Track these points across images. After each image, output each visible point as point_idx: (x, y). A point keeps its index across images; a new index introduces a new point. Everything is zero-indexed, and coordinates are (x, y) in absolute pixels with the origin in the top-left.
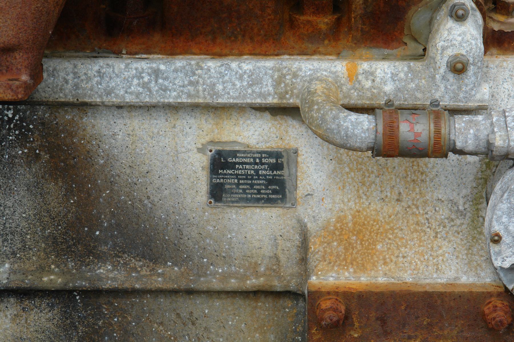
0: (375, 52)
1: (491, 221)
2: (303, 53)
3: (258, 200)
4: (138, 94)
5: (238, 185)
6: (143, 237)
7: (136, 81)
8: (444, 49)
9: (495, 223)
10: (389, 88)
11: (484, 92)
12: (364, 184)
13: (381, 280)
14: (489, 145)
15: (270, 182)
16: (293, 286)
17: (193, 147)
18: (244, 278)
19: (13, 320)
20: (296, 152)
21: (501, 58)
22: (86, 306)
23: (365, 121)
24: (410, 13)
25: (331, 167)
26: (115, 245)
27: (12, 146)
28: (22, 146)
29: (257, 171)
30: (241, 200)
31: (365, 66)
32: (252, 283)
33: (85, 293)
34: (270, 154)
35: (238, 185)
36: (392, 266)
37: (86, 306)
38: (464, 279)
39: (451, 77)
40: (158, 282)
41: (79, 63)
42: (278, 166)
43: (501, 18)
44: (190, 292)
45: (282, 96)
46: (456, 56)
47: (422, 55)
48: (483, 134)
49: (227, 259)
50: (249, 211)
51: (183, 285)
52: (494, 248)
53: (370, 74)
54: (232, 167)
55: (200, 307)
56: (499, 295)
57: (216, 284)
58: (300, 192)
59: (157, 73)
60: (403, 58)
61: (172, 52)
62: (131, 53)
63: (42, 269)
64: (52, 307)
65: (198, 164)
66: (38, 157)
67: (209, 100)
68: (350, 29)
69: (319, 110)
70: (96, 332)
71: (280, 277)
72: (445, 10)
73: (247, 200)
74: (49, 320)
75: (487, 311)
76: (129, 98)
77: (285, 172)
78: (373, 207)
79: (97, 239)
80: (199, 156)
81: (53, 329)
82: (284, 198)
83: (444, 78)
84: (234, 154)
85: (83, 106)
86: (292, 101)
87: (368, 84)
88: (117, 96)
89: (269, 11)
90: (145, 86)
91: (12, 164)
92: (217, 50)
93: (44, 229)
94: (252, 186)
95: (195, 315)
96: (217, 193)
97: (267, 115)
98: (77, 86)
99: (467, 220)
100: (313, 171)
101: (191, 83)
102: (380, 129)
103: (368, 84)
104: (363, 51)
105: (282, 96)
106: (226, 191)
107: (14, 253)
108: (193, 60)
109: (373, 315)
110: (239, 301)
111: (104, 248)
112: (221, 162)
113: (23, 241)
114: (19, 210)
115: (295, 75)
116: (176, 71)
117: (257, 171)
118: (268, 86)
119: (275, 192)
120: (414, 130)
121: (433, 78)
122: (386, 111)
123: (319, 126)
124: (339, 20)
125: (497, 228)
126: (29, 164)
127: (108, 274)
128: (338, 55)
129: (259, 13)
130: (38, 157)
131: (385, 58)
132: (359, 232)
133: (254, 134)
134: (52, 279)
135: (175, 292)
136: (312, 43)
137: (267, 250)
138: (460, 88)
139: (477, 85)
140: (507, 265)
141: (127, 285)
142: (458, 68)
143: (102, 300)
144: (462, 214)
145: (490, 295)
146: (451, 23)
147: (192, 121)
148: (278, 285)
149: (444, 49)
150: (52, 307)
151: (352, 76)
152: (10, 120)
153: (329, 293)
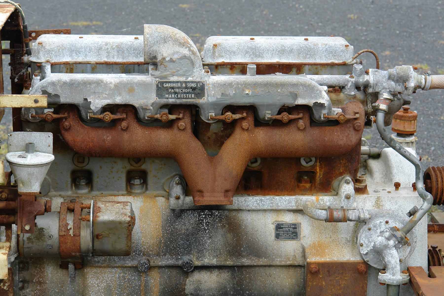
0: (323, 194)
1: (360, 240)
2: (302, 195)
3: (290, 238)
4: (256, 207)
5: (284, 234)
6: (256, 250)
7: (255, 203)
8: (344, 192)
9: (361, 240)
10: (328, 204)
11: (355, 205)
12: (320, 233)
13: (328, 260)
14: (359, 218)
15: (293, 233)
16: (301, 263)
17: (270, 223)
18: (286, 262)
19: (217, 276)
20: (300, 224)
21: (359, 195)
22: (238, 271)
23: (324, 212)
24: (333, 182)
25: (311, 228)
26: (247, 253)
27: (217, 223)
28: (220, 223)
29: (289, 230)
30: (285, 238)
31: (321, 197)
32: (288, 263)
33: (238, 267)
34: (293, 224)
35: (284, 234)
36: (331, 256)
37: (238, 271)
38: (352, 259)
39: (346, 200)
40: (261, 263)
41: (239, 198)
42: (295, 228)
43: (358, 184)
44: (270, 266)
45: (297, 207)
46: (347, 194)
47: (337, 194)
48: (357, 215)
49: (280, 256)
50: (287, 242)
51: (268, 264)
52: (361, 248)
53: (322, 200)
54: (282, 228)
55: (273, 271)
56: (362, 263)
57: (278, 263)
58: (302, 236)
59: (261, 200)
60: (331, 195)
61: (264, 195)
62: (253, 195)
63: (226, 260)
64: (228, 272)
65: (271, 228)
66: (225, 226)
67: (276, 208)
68: (315, 187)
69: (310, 209)
70: (241, 279)
71: (297, 261)
72: (343, 181)
73: (286, 238)
74: (228, 276)
75: (359, 267)
76: (253, 208)
77: (297, 230)
78: (323, 240)
79: (242, 251)
80: (272, 225)
81: (229, 279)
82: (297, 238)
83: (344, 200)
84: (282, 224)
85: (239, 210)
86: (300, 208)
87: (322, 203)
88: (250, 207)
89: (292, 182)
90: (258, 204)
91: (217, 228)
92: (277, 194)
93: (226, 248)
94: (288, 234)
95: (271, 274)
96: (277, 236)
97: (292, 213)
98: (238, 204)
99: (351, 243)
100: (306, 228)
101: (271, 203)
102: (328, 214)
103: (322, 203)
104: (319, 194)
105: (297, 207)
106: (280, 236)
107: (217, 256)
108: (272, 197)
109: (326, 270)
110: (284, 269)
111: (244, 254)
112: (279, 227)
113: (220, 252)
114: (219, 242)
115: (301, 200)
116: (267, 199)
117: (289, 230)
118: (293, 204)
119: (294, 236)
120: (337, 214)
121: (341, 200)
122: (330, 210)
123: (310, 214)
124: (312, 185)
125: (362, 242)
126: (222, 228)
127: (246, 261)
128: (312, 195)
129: (290, 183)
130: (225, 226)
131: (326, 195)
132: (320, 247)
133: (288, 219)
134: (229, 263)
135: (265, 266)
136: (304, 192)
137: (292, 254)
138: (348, 203)
139: (353, 203)
140: (365, 253)
141: (252, 264)
142: (348, 197)
143: (243, 269)
144: (349, 241)
145: (360, 263)
146: (345, 185)
147: (270, 215)
148: (296, 264)
149: (344, 192)
150: (228, 272)
151: (317, 200)
152: (217, 215)
153: (313, 263)
